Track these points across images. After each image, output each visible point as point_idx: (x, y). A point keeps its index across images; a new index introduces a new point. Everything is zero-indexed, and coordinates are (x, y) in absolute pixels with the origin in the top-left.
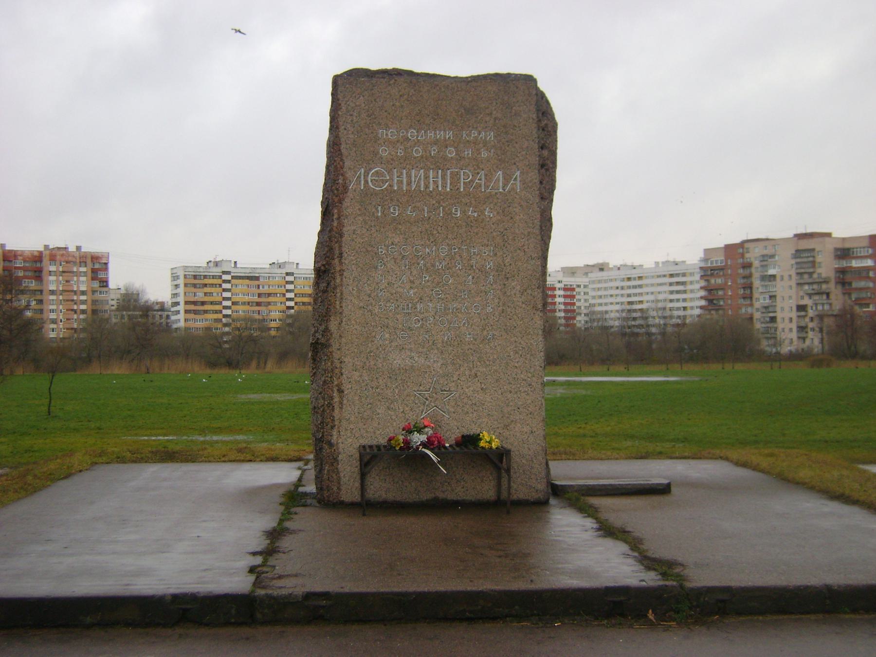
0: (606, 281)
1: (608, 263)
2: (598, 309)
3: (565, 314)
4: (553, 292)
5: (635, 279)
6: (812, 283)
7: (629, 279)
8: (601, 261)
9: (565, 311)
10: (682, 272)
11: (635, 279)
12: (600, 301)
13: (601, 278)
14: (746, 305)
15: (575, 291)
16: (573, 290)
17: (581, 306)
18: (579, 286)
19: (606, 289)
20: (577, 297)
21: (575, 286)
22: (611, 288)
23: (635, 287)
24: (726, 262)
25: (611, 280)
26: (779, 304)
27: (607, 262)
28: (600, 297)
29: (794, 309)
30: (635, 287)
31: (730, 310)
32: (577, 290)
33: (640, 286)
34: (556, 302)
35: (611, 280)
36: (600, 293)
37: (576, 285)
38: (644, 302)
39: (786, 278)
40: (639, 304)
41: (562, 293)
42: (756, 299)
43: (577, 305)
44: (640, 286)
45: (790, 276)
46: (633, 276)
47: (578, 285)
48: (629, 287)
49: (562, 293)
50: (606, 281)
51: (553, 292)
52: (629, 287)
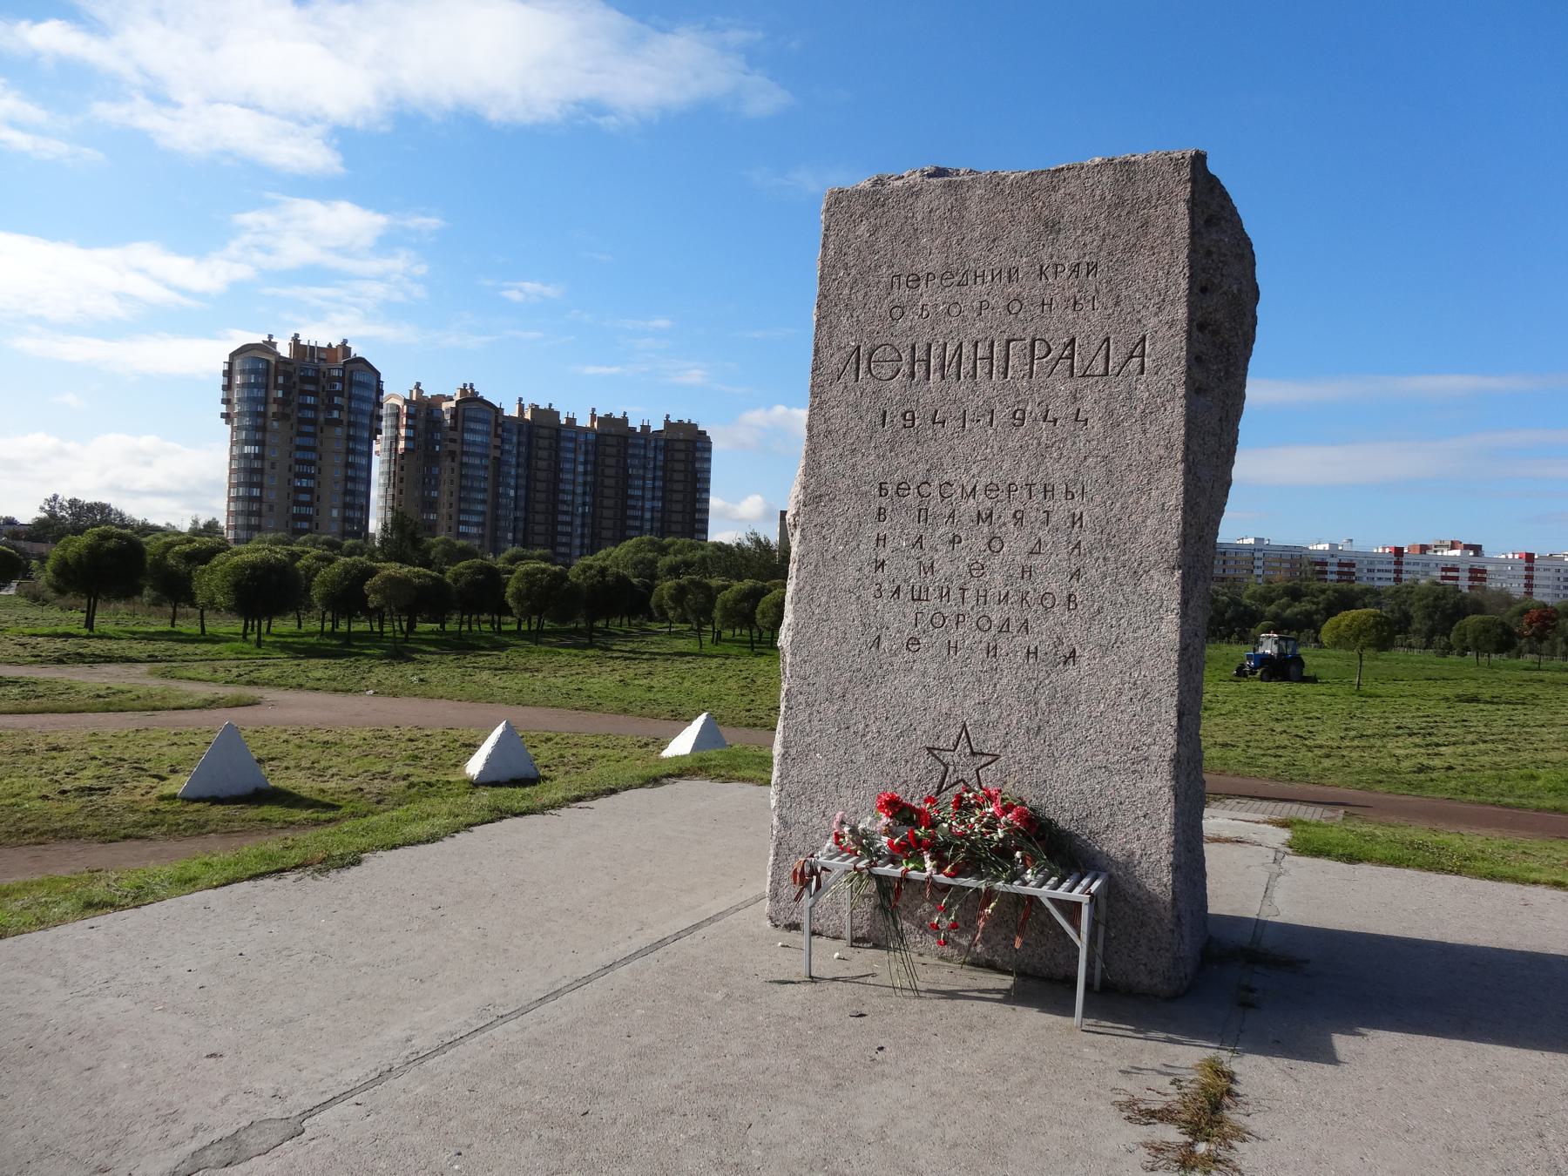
49: (1336, 569)
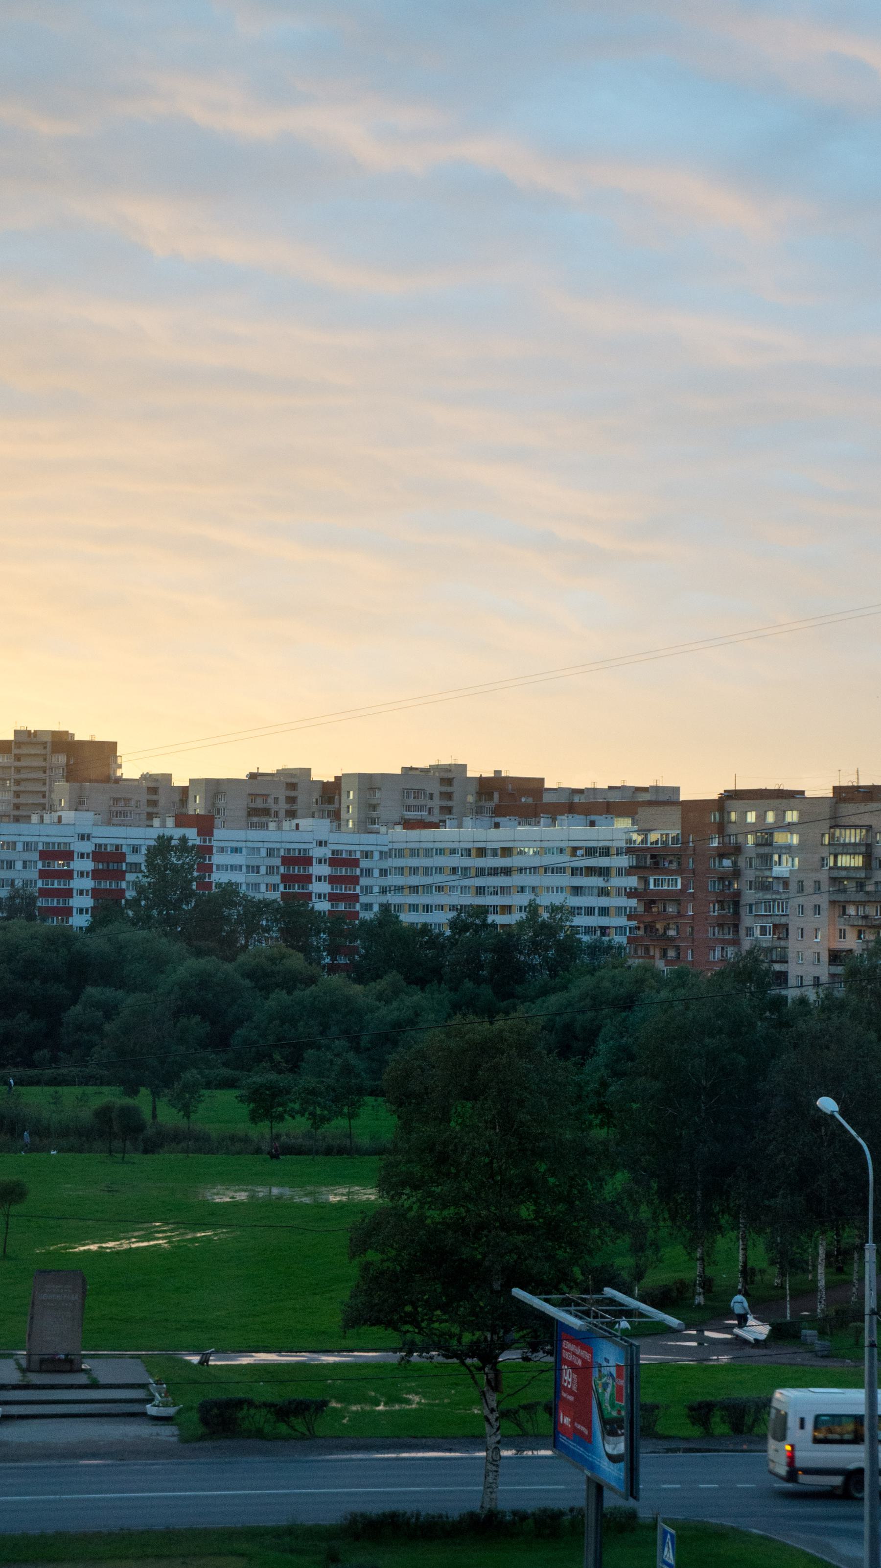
0: (428, 853)
1: (464, 767)
2: (407, 918)
3: (332, 906)
4: (304, 869)
5: (494, 853)
6: (863, 903)
7: (481, 852)
8: (446, 761)
9: (333, 880)
10: (601, 844)
11: (494, 853)
12: (413, 899)
13: (417, 846)
14: (724, 941)
15: (358, 866)
16: (355, 863)
17: (259, 884)
18: (367, 855)
19: (427, 871)
20: (364, 881)
21: (358, 856)
22: (440, 870)
23: (494, 872)
24: (685, 843)
25: (441, 852)
26: (794, 945)
27: (460, 762)
28: (414, 889)
29: (825, 957)
30: (494, 872)
31: (195, 883)
32: (364, 864)
33: (507, 871)
34: (310, 894)
35: (441, 852)
36: (414, 880)
37: (362, 851)
38: (515, 910)
39: (809, 886)
40: (503, 913)
41: (325, 870)
42: (747, 928)
43: (128, 861)
44: (507, 871)
45: (818, 883)
46: (489, 846)
47: (367, 853)
48: (480, 872)
49: (325, 870)
50: (428, 853)
51: (304, 869)
52: (480, 872)
